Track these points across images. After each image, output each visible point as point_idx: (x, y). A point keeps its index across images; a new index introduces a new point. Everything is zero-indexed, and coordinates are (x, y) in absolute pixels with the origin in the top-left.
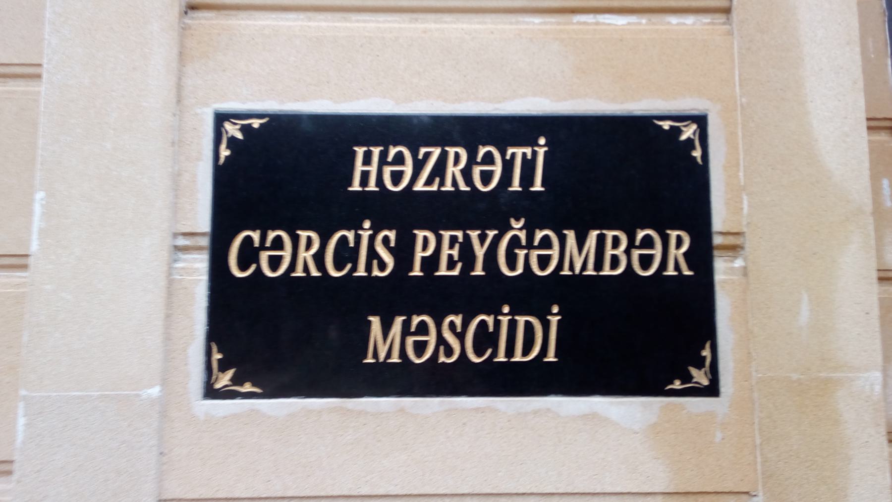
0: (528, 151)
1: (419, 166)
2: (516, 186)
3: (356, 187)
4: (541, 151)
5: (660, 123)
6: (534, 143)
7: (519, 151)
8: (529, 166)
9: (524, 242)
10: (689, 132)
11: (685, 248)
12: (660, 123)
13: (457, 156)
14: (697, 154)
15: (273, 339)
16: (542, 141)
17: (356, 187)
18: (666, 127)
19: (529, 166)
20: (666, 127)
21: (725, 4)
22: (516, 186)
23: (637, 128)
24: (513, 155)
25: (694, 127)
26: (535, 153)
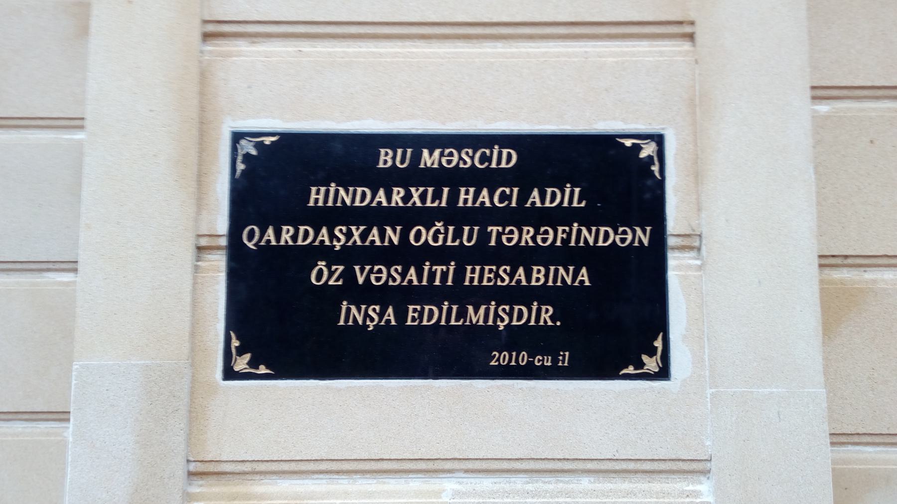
0: (444, 268)
1: (331, 274)
2: (532, 323)
3: (467, 283)
4: (452, 269)
5: (268, 371)
6: (447, 264)
7: (439, 268)
8: (444, 275)
9: (442, 231)
10: (241, 364)
11: (551, 312)
12: (268, 371)
13: (288, 231)
14: (235, 343)
15: (616, 178)
16: (453, 263)
17: (467, 283)
18: (262, 367)
19: (444, 275)
20: (262, 367)
21: (196, 488)
22: (532, 323)
23: (285, 369)
24: (433, 202)
25: (236, 368)
26: (448, 269)
